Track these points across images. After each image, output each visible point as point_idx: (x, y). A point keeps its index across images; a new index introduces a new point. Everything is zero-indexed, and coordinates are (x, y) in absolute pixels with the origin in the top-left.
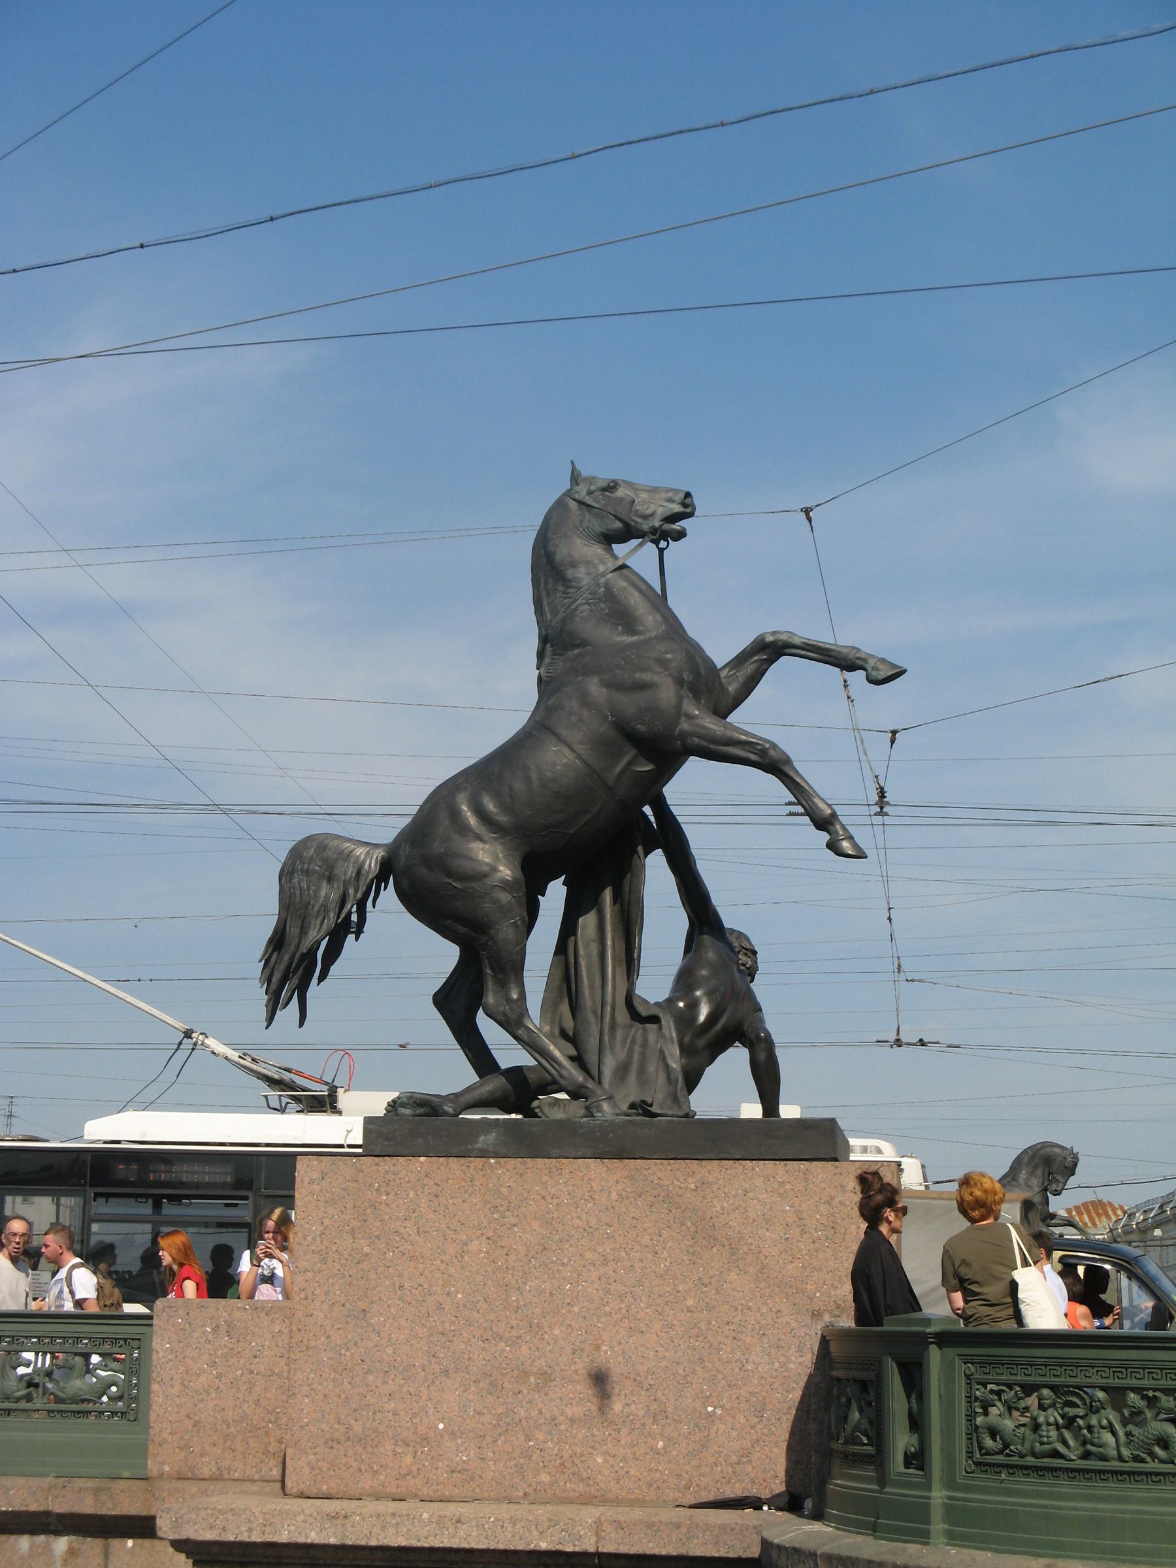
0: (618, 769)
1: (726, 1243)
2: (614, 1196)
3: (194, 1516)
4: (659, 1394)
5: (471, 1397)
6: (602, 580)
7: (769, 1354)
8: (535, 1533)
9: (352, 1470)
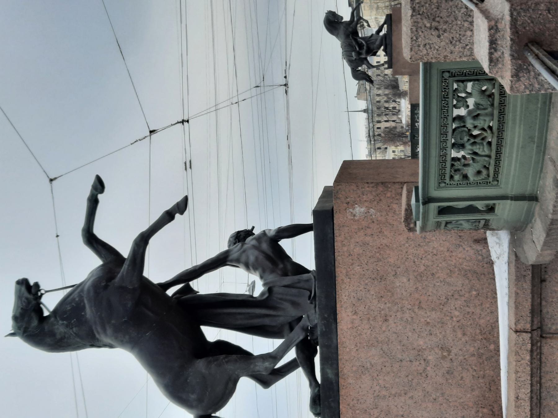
0: (150, 314)
1: (375, 263)
4: (449, 294)
5: (454, 382)
7: (429, 242)
8: (522, 362)
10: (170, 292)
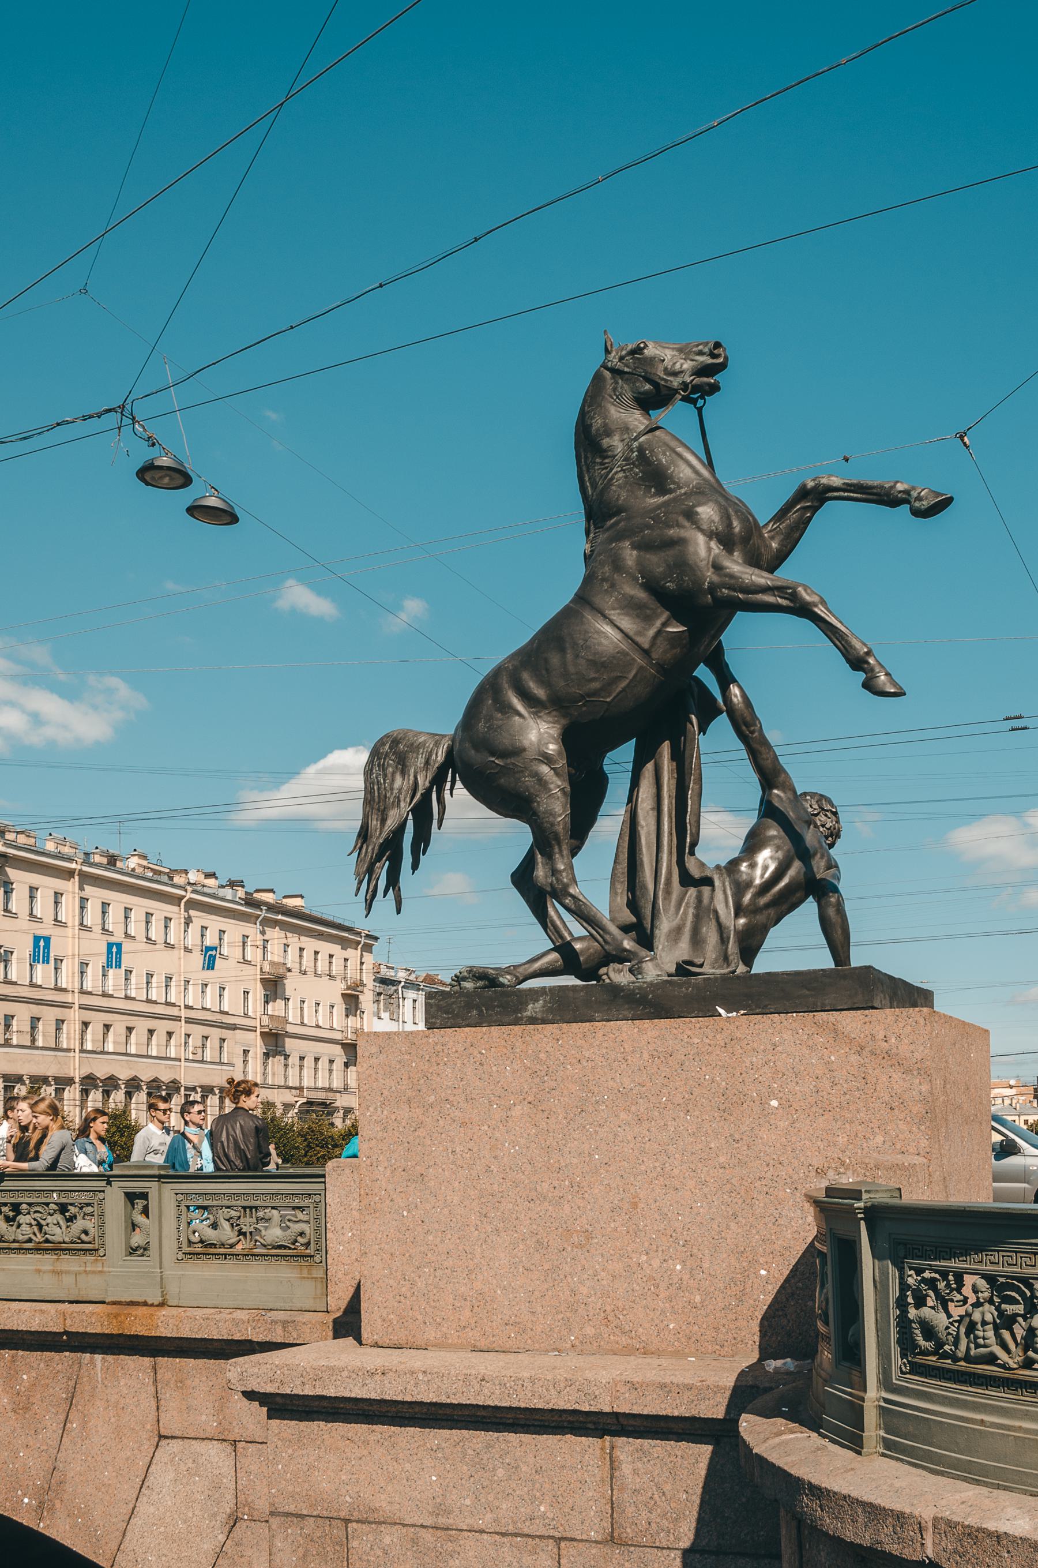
2: (646, 1056)
3: (256, 1370)
6: (636, 444)
9: (417, 1322)
10: (703, 673)
